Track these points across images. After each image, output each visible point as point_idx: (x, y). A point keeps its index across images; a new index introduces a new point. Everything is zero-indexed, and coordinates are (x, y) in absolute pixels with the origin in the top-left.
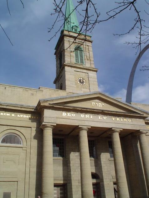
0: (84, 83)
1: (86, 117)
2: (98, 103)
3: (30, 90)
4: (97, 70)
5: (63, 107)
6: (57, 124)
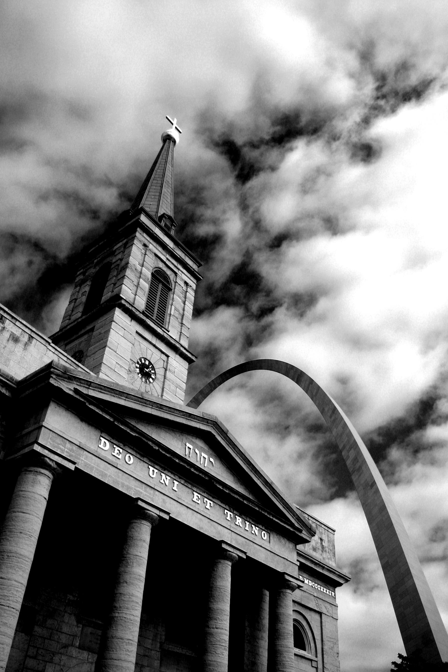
0: (151, 380)
1: (162, 481)
2: (201, 450)
3: (14, 321)
4: (194, 358)
6: (76, 468)
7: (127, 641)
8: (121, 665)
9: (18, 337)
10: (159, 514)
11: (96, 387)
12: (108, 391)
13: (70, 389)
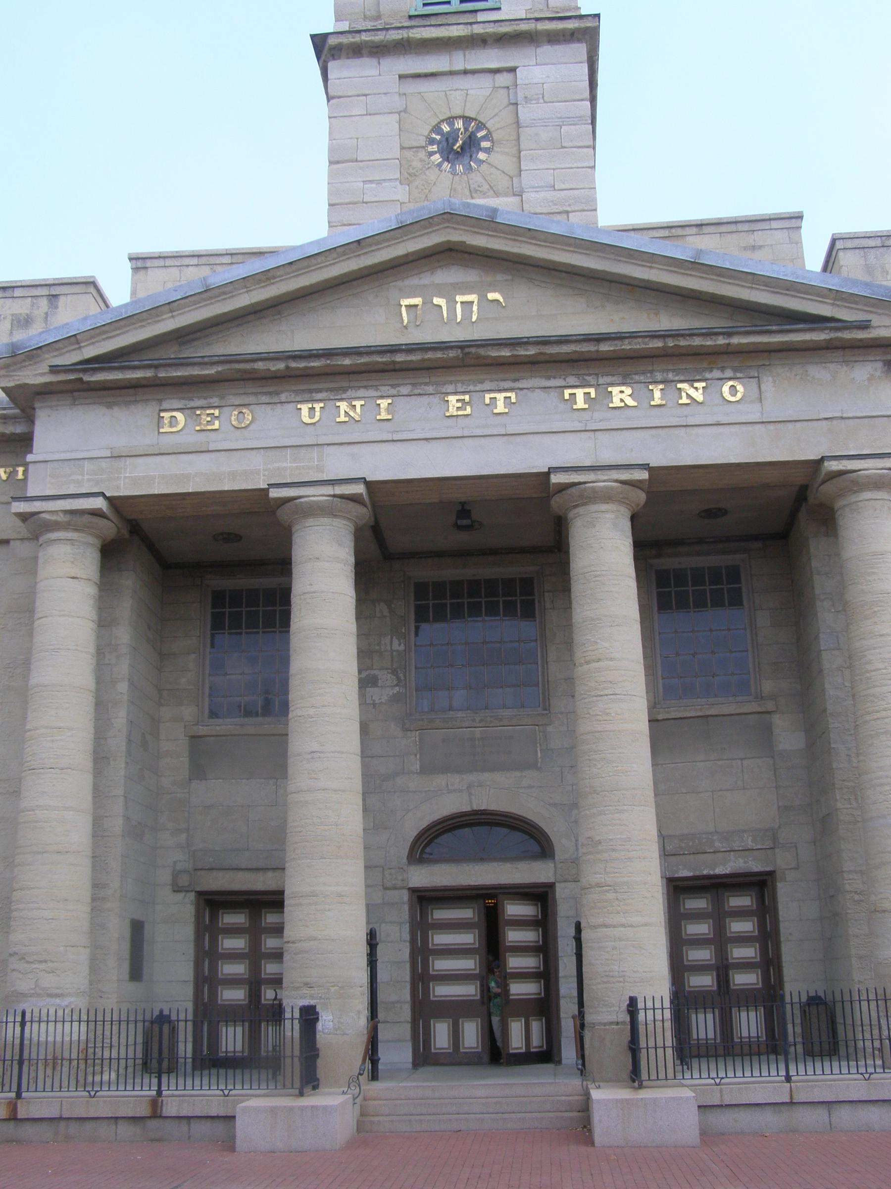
5: (149, 373)
7: (309, 756)
8: (302, 799)
9: (27, 315)
10: (332, 493)
11: (92, 337)
12: (125, 326)
13: (43, 374)
